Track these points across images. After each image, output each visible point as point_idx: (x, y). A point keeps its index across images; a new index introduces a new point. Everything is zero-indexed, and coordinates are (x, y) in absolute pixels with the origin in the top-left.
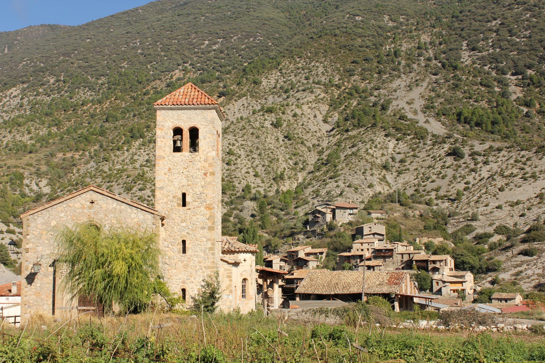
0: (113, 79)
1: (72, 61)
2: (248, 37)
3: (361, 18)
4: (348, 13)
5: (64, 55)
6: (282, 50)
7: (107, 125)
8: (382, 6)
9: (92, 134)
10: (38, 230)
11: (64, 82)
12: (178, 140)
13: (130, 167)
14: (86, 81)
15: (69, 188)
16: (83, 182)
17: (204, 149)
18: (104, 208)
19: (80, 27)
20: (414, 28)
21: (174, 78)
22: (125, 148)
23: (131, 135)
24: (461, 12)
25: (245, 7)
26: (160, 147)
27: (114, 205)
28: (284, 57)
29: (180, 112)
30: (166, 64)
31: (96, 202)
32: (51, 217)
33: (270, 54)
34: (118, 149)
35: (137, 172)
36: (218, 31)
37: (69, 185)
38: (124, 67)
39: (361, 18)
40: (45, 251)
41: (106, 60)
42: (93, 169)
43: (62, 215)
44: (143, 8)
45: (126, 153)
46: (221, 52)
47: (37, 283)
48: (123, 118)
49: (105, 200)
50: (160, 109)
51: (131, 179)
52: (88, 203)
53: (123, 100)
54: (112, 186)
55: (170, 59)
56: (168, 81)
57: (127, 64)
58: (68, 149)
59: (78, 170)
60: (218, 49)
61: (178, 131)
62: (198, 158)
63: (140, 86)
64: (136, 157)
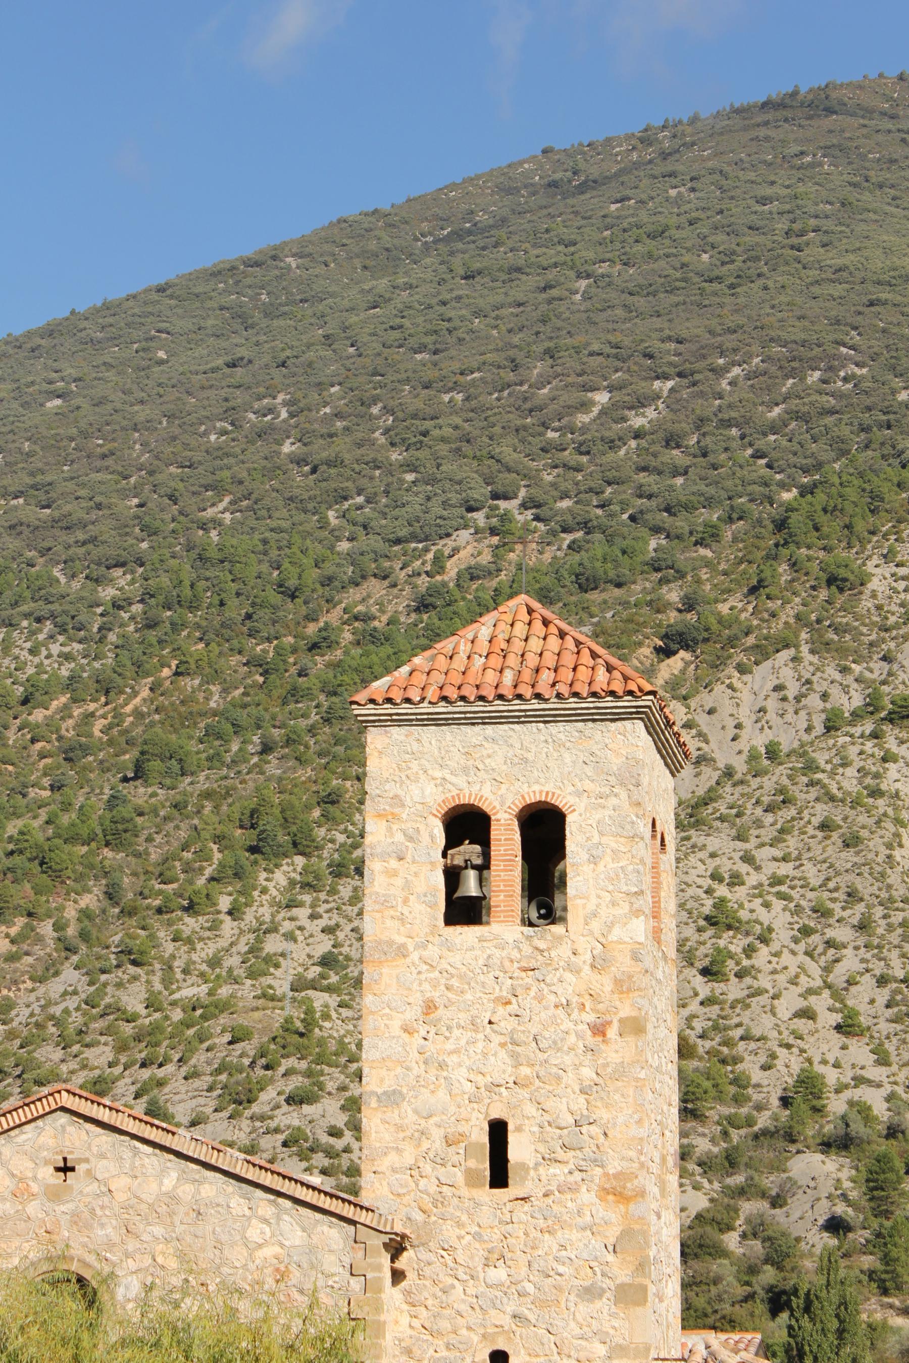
0: (165, 580)
2: (794, 366)
7: (139, 794)
12: (468, 864)
13: (247, 991)
14: (41, 591)
17: (591, 907)
18: (120, 1197)
21: (452, 568)
22: (225, 903)
23: (250, 838)
25: (782, 225)
26: (385, 903)
27: (169, 1183)
29: (474, 734)
30: (415, 504)
31: (81, 1168)
34: (190, 909)
35: (279, 1017)
36: (656, 345)
38: (217, 523)
41: (136, 491)
42: (71, 1003)
44: (303, 250)
45: (228, 926)
46: (672, 441)
48: (214, 760)
49: (127, 1154)
51: (249, 1047)
52: (47, 1174)
53: (216, 675)
55: (432, 481)
56: (423, 582)
57: (234, 506)
60: (657, 426)
63: (291, 610)
64: (273, 944)
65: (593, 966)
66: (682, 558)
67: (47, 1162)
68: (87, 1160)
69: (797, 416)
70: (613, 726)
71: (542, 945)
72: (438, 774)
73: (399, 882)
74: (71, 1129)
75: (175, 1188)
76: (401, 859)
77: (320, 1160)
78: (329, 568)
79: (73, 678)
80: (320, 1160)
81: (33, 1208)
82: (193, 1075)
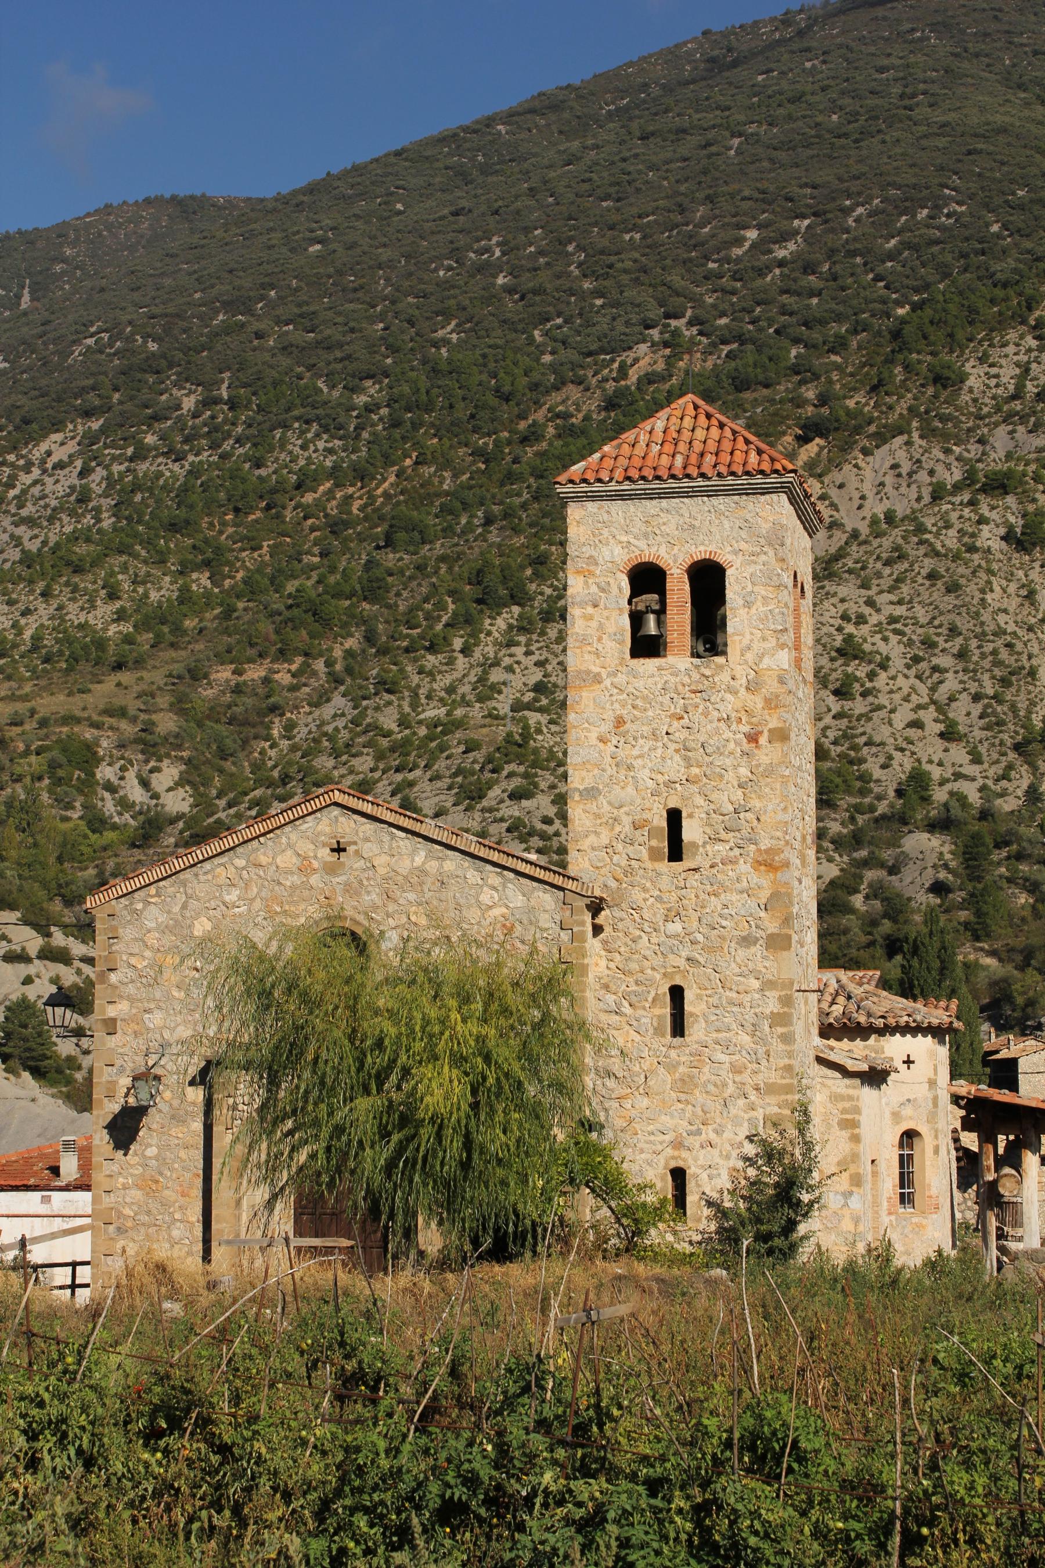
0: (406, 389)
1: (257, 326)
5: (228, 306)
7: (389, 559)
9: (338, 595)
10: (148, 954)
11: (233, 404)
12: (648, 610)
13: (477, 712)
14: (309, 398)
15: (258, 793)
17: (746, 642)
18: (382, 871)
19: (283, 200)
21: (633, 375)
22: (458, 643)
26: (584, 641)
27: (419, 860)
29: (652, 506)
30: (603, 323)
31: (351, 849)
34: (432, 649)
35: (501, 732)
38: (446, 342)
40: (173, 1030)
42: (340, 723)
43: (232, 896)
44: (510, 117)
45: (461, 662)
46: (809, 268)
47: (149, 1145)
48: (448, 531)
49: (386, 838)
50: (579, 498)
51: (479, 756)
52: (325, 853)
53: (446, 464)
54: (411, 784)
55: (616, 304)
56: (610, 386)
58: (252, 652)
59: (290, 727)
60: (797, 256)
61: (647, 578)
62: (725, 677)
63: (506, 412)
64: (496, 676)
65: (748, 689)
67: (324, 845)
70: (762, 498)
71: (708, 672)
72: (624, 539)
74: (342, 819)
77: (536, 842)
78: (536, 376)
79: (336, 467)
80: (536, 842)
81: (315, 880)
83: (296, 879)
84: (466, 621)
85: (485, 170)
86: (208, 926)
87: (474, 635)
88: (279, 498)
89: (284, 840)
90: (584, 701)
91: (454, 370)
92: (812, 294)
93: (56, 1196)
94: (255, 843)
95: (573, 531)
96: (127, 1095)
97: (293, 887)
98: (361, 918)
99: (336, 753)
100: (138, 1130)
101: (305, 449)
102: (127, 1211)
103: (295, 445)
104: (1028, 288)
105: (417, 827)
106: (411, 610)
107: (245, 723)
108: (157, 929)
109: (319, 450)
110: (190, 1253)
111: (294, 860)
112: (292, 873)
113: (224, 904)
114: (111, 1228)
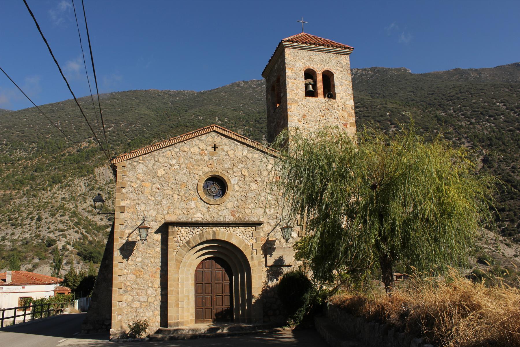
0: (41, 145)
1: (12, 132)
2: (131, 124)
3: (202, 118)
4: (194, 114)
5: (7, 128)
6: (153, 133)
7: (36, 174)
8: (214, 112)
9: (26, 179)
10: (138, 182)
11: (6, 145)
12: (310, 83)
13: (54, 201)
14: (22, 145)
15: (8, 213)
16: (19, 210)
17: (341, 96)
18: (231, 156)
19: (19, 111)
20: (233, 125)
21: (82, 147)
22: (49, 189)
23: (53, 181)
24: (260, 119)
25: (129, 106)
26: (292, 90)
27: (245, 152)
28: (154, 137)
29: (311, 53)
30: (78, 137)
31: (220, 147)
32: (157, 164)
33: (145, 135)
34: (44, 190)
35: (59, 204)
36: (112, 120)
37: (9, 212)
38: (49, 138)
39: (202, 118)
40: (148, 212)
41: (37, 133)
42: (25, 202)
43: (173, 162)
44: (62, 103)
45: (49, 193)
46: (114, 132)
47: (137, 257)
48: (47, 170)
49: (233, 145)
50: (288, 47)
51: (54, 208)
52: (210, 148)
53: (47, 159)
54: (41, 213)
55: (80, 135)
56: (78, 148)
57: (51, 136)
58: (7, 188)
59: (15, 202)
60: (112, 130)
61: (309, 74)
62: (336, 105)
63: (59, 151)
64: (56, 195)
65: (343, 110)
66: (115, 148)
67: (210, 145)
68: (221, 146)
69: (131, 131)
70: (343, 56)
71: (331, 104)
72: (303, 61)
73: (295, 85)
74: (216, 137)
75: (247, 154)
76: (295, 79)
77: (65, 224)
78: (65, 145)
79: (26, 157)
80: (65, 224)
81: (206, 158)
82: (46, 212)
83: (199, 157)
84: (50, 185)
85: (58, 111)
86: (164, 172)
87: (52, 188)
88: (14, 162)
89: (194, 143)
90: (293, 108)
91: (50, 143)
92: (114, 136)
93: (4, 287)
94: (183, 143)
95: (287, 56)
96: (128, 237)
97: (197, 160)
98: (224, 172)
99: (25, 207)
100: (133, 251)
101: (20, 154)
102: (128, 284)
103: (18, 153)
104: (151, 139)
105: (245, 141)
106: (40, 183)
107: (5, 201)
108: (143, 173)
109: (23, 154)
110: (156, 300)
111: (198, 150)
112: (197, 155)
113: (170, 164)
114: (121, 291)
